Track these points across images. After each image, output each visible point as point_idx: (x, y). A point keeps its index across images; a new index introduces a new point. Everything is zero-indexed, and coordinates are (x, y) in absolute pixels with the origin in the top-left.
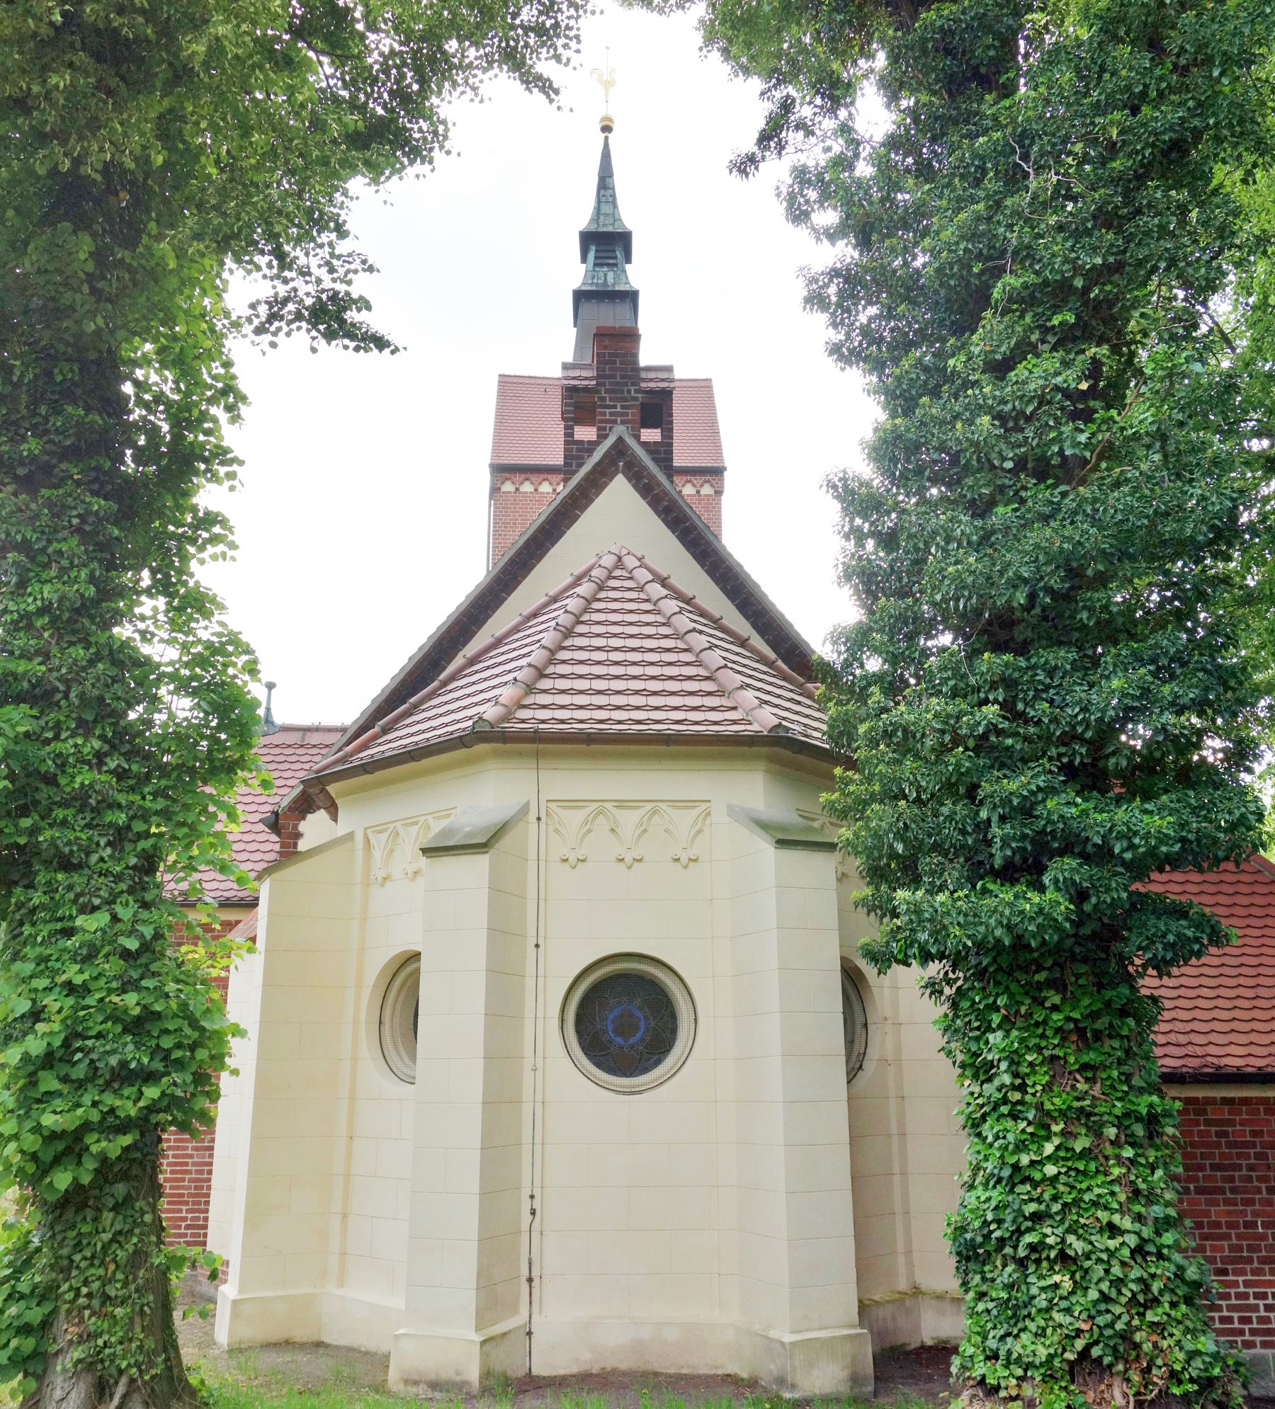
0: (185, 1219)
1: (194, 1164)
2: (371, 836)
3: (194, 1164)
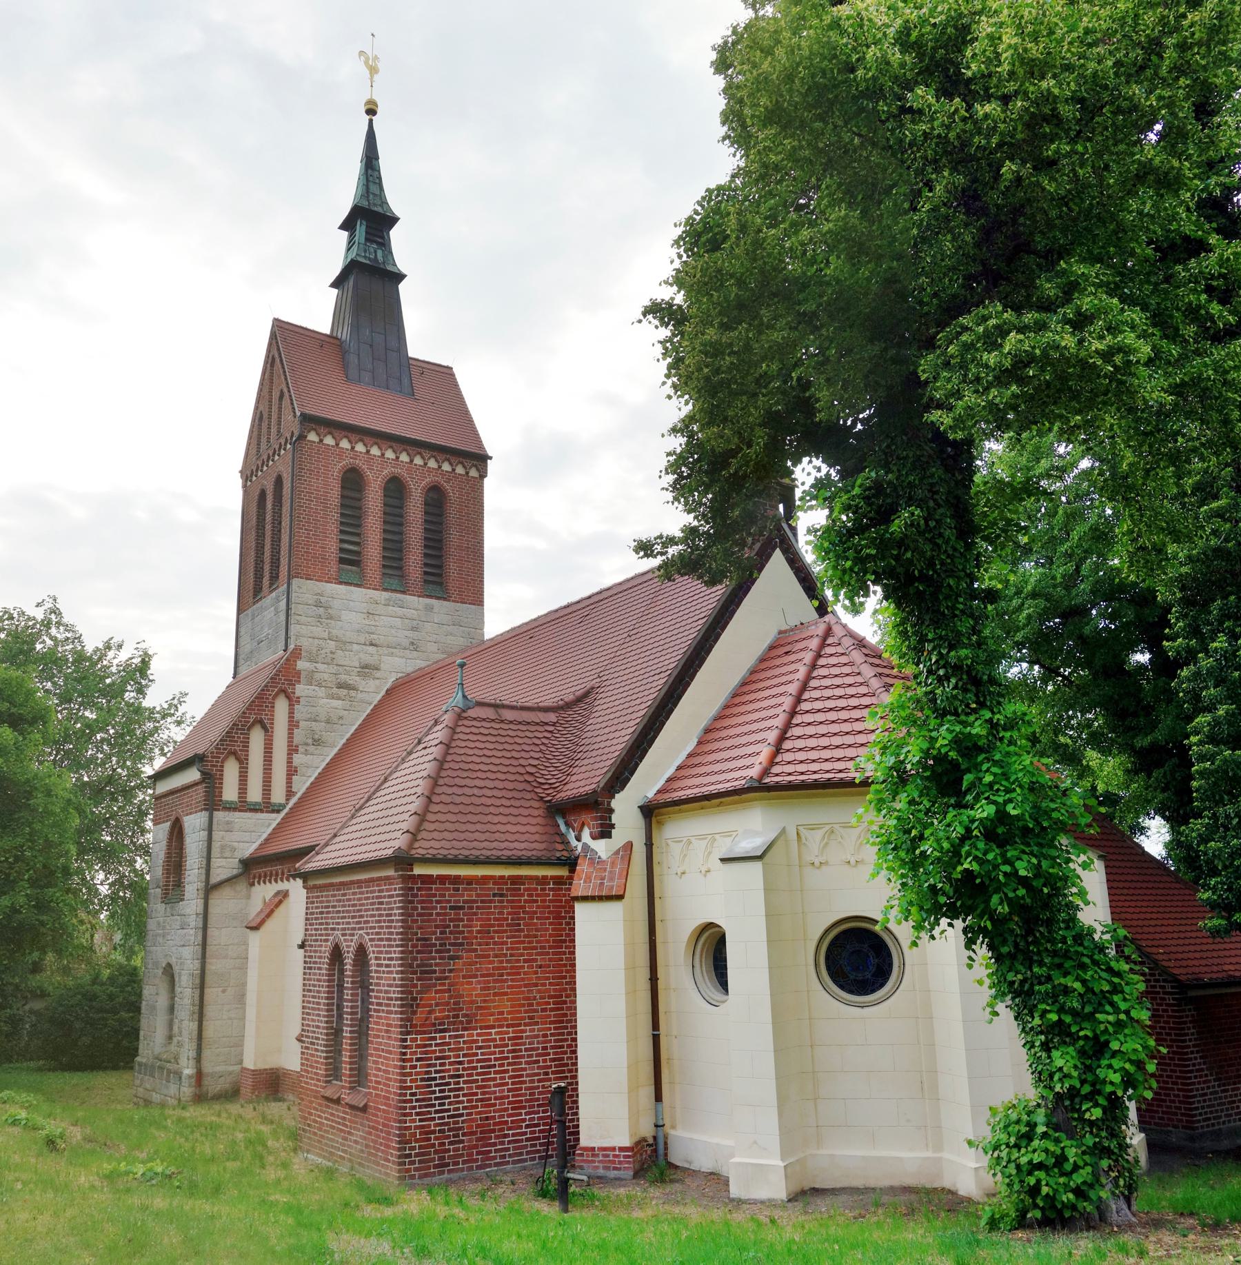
0: (524, 1120)
1: (528, 1075)
2: (803, 831)
3: (528, 1075)
